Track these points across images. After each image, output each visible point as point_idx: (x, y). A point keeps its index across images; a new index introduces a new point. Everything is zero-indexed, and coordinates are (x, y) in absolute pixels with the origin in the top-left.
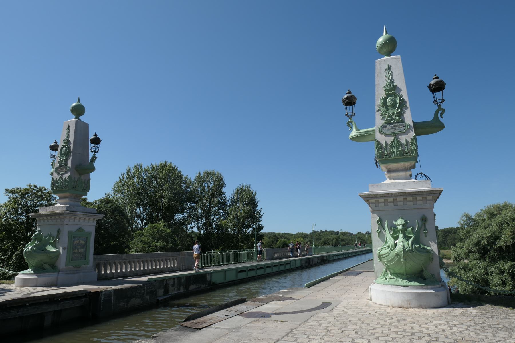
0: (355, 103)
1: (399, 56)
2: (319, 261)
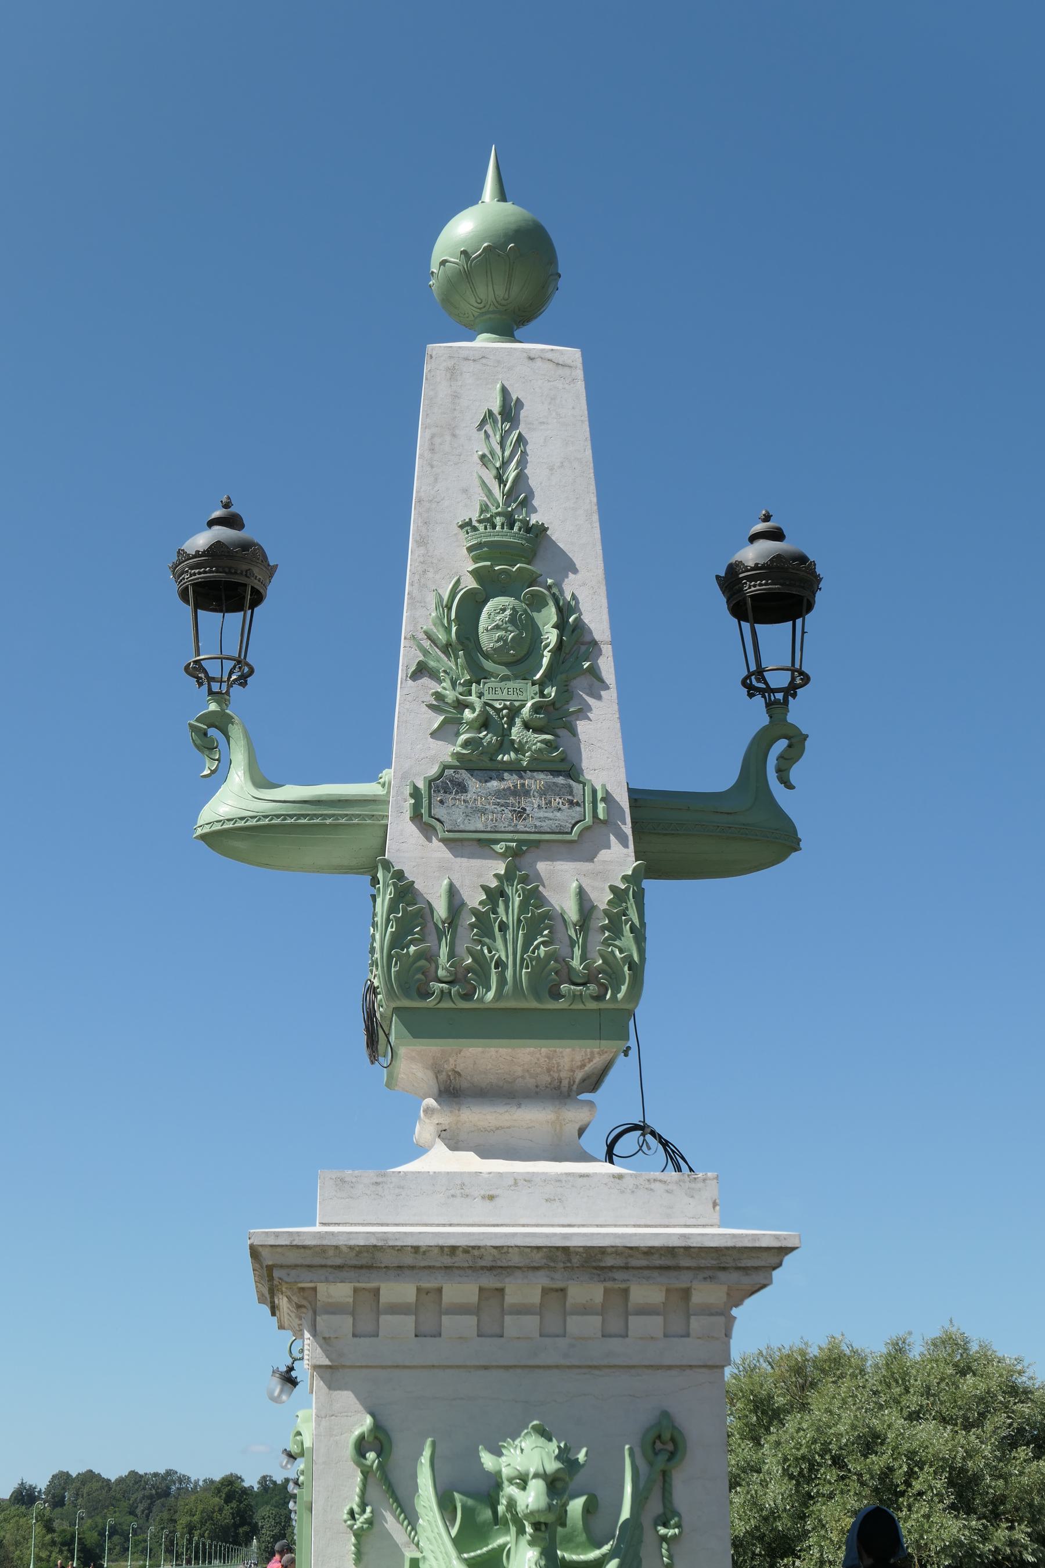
0: (258, 598)
1: (573, 355)
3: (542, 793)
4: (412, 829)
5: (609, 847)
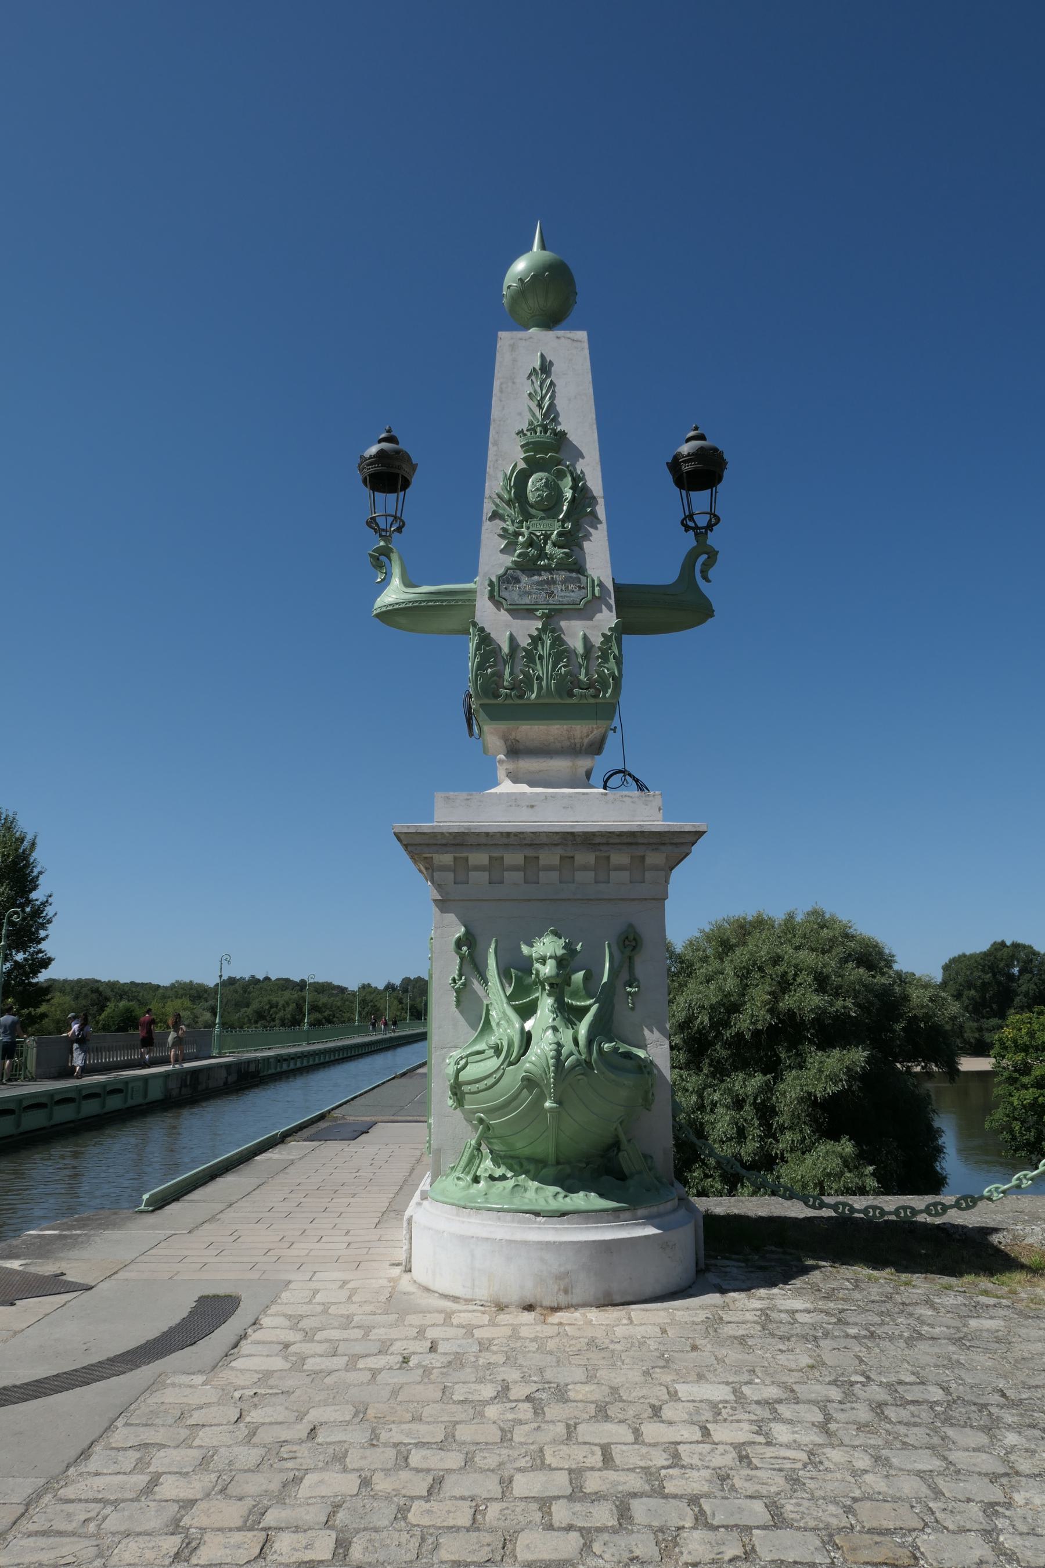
0: (406, 484)
1: (582, 335)
2: (232, 1078)
3: (563, 582)
4: (489, 604)
5: (601, 612)
